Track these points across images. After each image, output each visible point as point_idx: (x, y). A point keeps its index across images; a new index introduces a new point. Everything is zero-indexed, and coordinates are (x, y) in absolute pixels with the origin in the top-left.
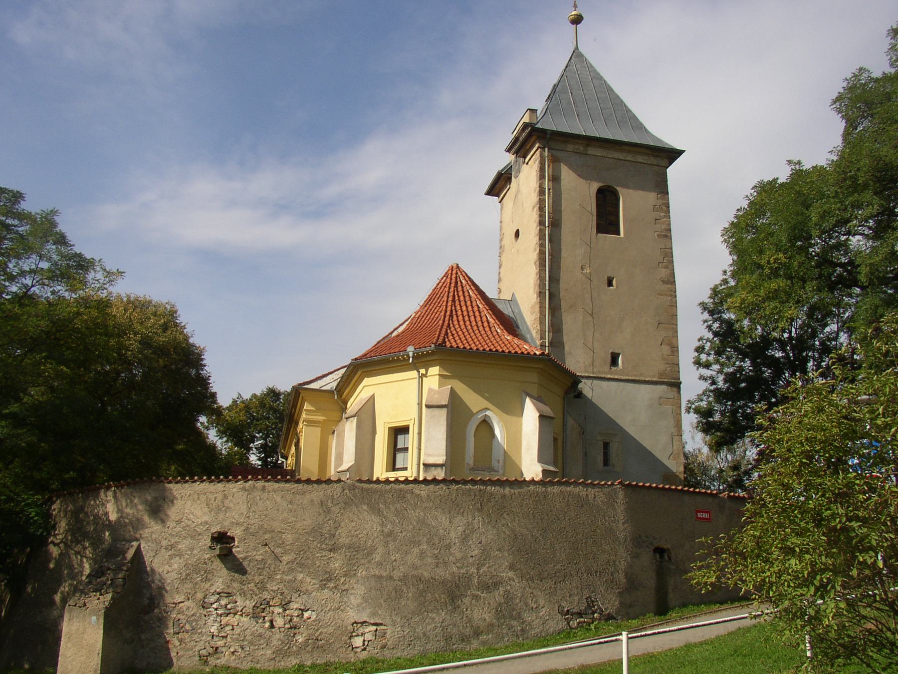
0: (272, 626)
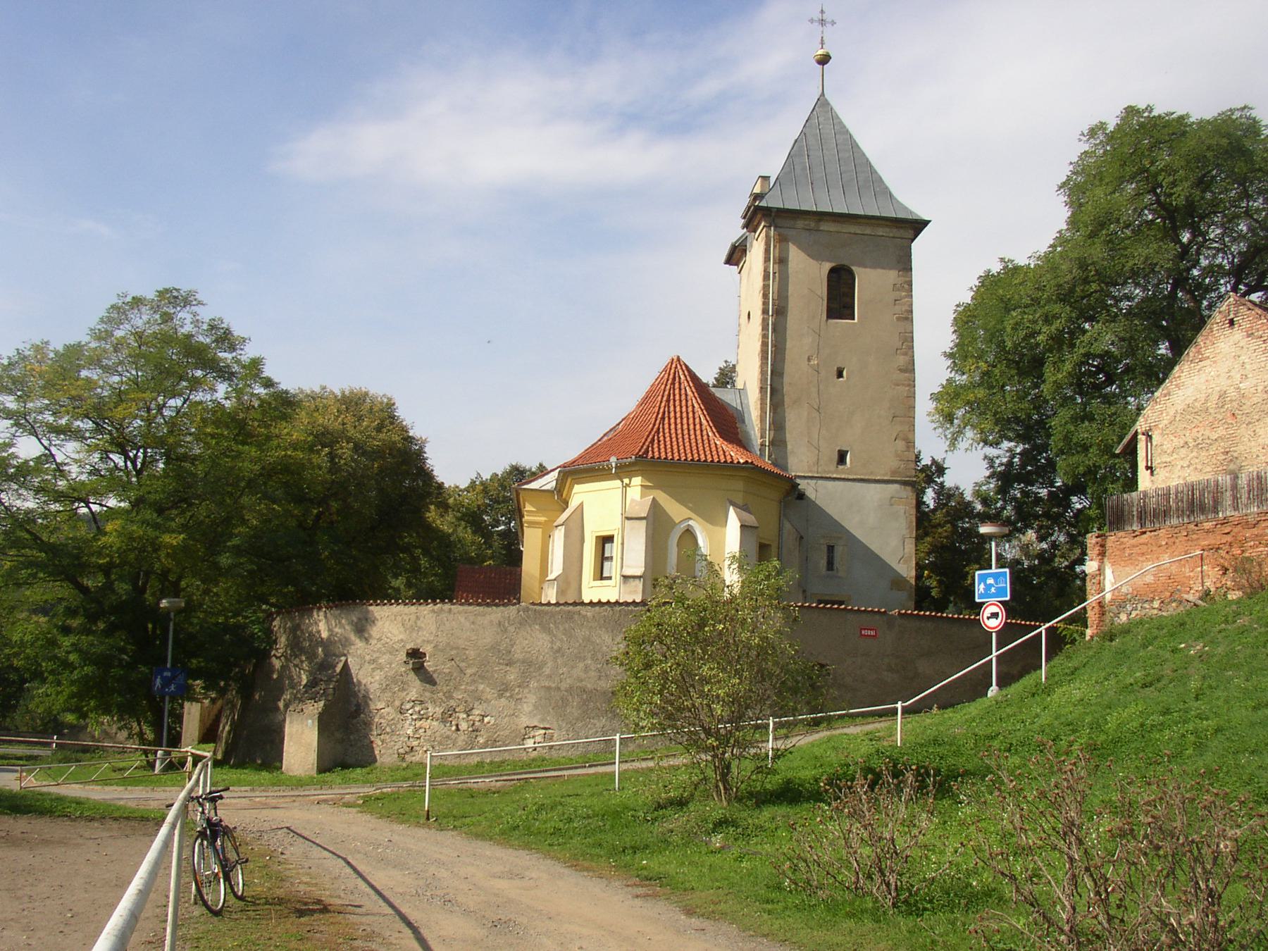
0: (458, 729)
